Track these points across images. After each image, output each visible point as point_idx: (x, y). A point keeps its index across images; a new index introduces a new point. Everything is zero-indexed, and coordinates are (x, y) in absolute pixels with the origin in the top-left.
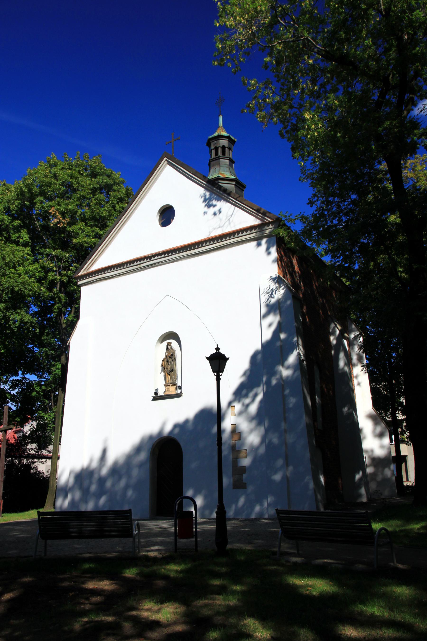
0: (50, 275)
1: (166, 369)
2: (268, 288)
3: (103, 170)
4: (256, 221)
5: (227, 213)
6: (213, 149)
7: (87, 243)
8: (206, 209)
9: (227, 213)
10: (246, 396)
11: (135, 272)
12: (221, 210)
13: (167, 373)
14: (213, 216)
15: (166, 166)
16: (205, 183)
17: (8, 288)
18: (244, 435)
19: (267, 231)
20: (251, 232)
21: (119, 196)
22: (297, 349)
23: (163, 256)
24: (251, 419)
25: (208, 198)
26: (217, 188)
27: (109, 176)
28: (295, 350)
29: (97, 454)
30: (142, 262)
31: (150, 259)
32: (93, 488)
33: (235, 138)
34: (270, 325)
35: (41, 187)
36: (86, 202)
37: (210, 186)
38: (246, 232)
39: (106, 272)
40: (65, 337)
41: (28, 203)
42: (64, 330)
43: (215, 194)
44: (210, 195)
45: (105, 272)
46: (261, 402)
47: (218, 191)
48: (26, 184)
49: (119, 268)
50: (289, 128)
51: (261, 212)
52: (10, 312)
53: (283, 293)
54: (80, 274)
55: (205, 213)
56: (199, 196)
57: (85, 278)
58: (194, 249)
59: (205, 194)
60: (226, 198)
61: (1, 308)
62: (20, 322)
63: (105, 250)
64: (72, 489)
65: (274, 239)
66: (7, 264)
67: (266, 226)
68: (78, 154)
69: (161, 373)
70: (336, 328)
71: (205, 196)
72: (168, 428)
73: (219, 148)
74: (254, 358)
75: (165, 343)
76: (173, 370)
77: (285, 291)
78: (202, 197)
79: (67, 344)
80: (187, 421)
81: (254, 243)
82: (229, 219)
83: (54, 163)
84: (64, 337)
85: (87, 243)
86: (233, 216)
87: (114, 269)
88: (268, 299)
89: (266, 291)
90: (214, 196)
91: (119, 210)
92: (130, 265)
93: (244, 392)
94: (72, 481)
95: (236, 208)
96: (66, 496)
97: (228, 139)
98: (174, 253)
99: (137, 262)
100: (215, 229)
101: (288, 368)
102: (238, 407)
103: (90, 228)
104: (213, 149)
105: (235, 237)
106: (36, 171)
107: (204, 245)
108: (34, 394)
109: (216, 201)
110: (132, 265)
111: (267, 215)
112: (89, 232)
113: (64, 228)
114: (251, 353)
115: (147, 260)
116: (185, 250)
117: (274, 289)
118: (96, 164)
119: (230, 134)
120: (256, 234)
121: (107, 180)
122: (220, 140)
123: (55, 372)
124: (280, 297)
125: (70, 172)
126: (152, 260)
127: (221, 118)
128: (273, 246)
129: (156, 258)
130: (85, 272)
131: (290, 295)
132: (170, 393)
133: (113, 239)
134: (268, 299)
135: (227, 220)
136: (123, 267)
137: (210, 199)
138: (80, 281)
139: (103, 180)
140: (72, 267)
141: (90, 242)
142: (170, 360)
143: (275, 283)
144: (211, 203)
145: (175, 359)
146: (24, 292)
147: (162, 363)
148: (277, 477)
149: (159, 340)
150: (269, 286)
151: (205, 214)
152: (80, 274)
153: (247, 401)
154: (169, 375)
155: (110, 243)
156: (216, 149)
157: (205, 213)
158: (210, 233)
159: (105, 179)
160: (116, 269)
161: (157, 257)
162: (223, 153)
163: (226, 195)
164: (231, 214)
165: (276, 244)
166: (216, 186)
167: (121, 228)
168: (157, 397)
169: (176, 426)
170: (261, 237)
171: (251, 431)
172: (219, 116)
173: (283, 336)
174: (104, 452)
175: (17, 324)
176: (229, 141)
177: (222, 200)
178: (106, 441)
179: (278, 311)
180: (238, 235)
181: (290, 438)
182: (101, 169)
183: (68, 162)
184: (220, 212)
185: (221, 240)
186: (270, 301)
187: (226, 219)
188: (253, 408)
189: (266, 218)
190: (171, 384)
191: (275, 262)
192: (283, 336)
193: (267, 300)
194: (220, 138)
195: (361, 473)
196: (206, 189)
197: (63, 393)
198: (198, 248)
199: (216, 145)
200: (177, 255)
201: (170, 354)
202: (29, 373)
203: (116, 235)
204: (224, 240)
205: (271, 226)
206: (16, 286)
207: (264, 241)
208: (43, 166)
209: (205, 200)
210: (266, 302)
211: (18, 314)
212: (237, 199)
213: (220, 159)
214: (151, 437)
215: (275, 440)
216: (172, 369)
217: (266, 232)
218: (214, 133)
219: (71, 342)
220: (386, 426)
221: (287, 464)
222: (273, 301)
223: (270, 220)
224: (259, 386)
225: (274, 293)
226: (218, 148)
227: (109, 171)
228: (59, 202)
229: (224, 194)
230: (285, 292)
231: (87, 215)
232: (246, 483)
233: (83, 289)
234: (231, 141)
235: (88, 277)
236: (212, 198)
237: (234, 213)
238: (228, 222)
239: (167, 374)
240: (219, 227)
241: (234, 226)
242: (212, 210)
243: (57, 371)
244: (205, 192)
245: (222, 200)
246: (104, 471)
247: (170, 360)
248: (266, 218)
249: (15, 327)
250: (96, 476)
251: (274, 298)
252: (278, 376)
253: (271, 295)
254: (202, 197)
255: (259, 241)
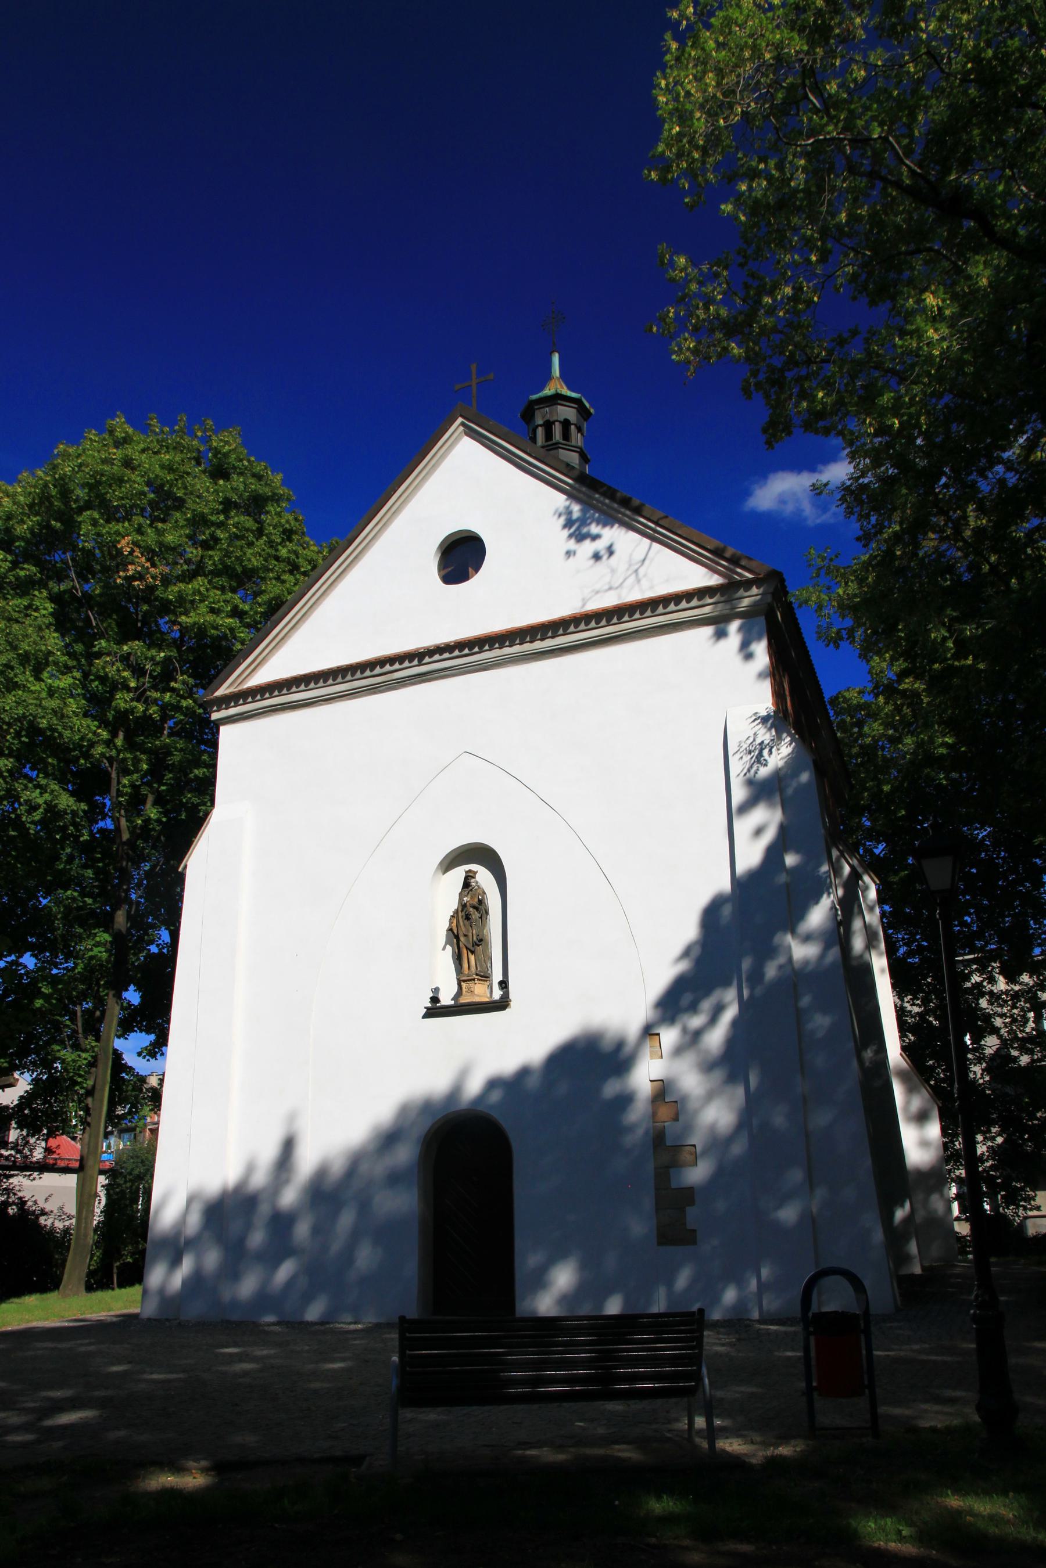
0: (120, 699)
1: (462, 939)
2: (751, 739)
3: (246, 463)
4: (711, 577)
5: (631, 555)
6: (541, 426)
7: (216, 628)
8: (572, 544)
9: (631, 555)
10: (693, 1008)
11: (375, 693)
12: (615, 548)
13: (467, 948)
14: (592, 561)
15: (461, 439)
16: (570, 481)
17: (19, 719)
18: (692, 1105)
19: (746, 602)
20: (700, 603)
21: (287, 526)
22: (829, 894)
23: (456, 653)
24: (708, 1067)
25: (577, 520)
26: (604, 495)
27: (259, 477)
28: (825, 896)
29: (268, 1152)
30: (397, 666)
31: (420, 661)
32: (257, 1238)
33: (591, 405)
34: (758, 832)
35: (91, 487)
36: (207, 532)
37: (584, 489)
38: (688, 602)
39: (294, 689)
40: (127, 865)
41: (59, 525)
42: (125, 847)
43: (596, 509)
44: (583, 511)
45: (292, 691)
46: (735, 1023)
47: (607, 501)
48: (57, 476)
49: (330, 682)
50: (762, 377)
51: (728, 555)
52: (22, 783)
53: (789, 755)
54: (218, 693)
55: (569, 554)
56: (552, 512)
57: (232, 704)
58: (542, 640)
59: (568, 508)
60: (627, 519)
61: (4, 769)
62: (45, 809)
63: (290, 637)
64: (191, 1243)
65: (761, 621)
66: (24, 659)
67: (742, 590)
68: (181, 419)
69: (444, 949)
70: (843, 861)
71: (569, 512)
72: (474, 1087)
73: (557, 424)
74: (711, 915)
75: (458, 874)
76: (481, 940)
77: (794, 749)
78: (560, 515)
79: (180, 870)
80: (524, 1072)
81: (708, 631)
82: (636, 571)
83: (123, 435)
84: (124, 864)
85: (216, 628)
86: (647, 562)
87: (316, 683)
88: (751, 767)
89: (744, 748)
90: (594, 514)
91: (289, 558)
92: (362, 673)
93: (686, 999)
94: (194, 1220)
95: (656, 546)
96: (176, 1262)
97: (576, 406)
98: (487, 647)
99: (381, 667)
100: (597, 592)
101: (807, 938)
102: (669, 1036)
103: (219, 593)
104: (541, 426)
105: (657, 612)
106: (80, 451)
107: (572, 629)
108: (39, 1003)
109: (600, 527)
110: (368, 673)
111: (743, 563)
112: (219, 602)
113: (152, 589)
114: (704, 899)
115: (410, 662)
116: (539, 637)
117: (766, 742)
118: (230, 446)
119: (583, 395)
120: (714, 608)
121: (254, 486)
122: (559, 407)
123: (90, 953)
124: (781, 764)
125: (168, 457)
126: (424, 662)
127: (556, 359)
128: (759, 639)
129: (437, 657)
130: (231, 690)
131: (808, 759)
132: (477, 999)
133: (311, 610)
134: (751, 767)
135: (630, 572)
136: (343, 678)
137: (583, 521)
138: (218, 711)
139: (245, 484)
140: (176, 682)
141: (221, 625)
142: (475, 915)
143: (770, 729)
144: (585, 530)
145: (487, 913)
146: (61, 735)
147: (451, 922)
148: (788, 1214)
149: (441, 863)
150: (755, 734)
151: (569, 557)
152: (220, 692)
153: (696, 1021)
154: (473, 952)
155: (304, 618)
156: (548, 426)
157: (569, 554)
158: (584, 603)
159: (251, 483)
160: (321, 684)
161: (440, 655)
162: (566, 436)
163: (628, 513)
164: (642, 557)
165: (766, 634)
166: (601, 490)
167: (336, 583)
168: (435, 1010)
169: (493, 1084)
170: (727, 615)
171: (710, 1096)
172: (553, 352)
173: (790, 860)
174: (288, 1146)
175: (37, 816)
176: (578, 411)
177: (617, 525)
178: (292, 1118)
179: (778, 799)
180: (665, 607)
181: (821, 1119)
182: (241, 460)
183: (160, 437)
184: (610, 551)
185: (619, 619)
186: (756, 773)
187: (628, 569)
188: (716, 1038)
189: (739, 570)
190: (477, 975)
191: (766, 677)
192: (790, 860)
193: (749, 770)
194: (559, 402)
195: (907, 1205)
196: (570, 495)
197: (117, 1003)
198: (553, 637)
199: (548, 417)
200: (496, 653)
201: (476, 900)
202: (15, 953)
203: (322, 599)
204: (626, 618)
205: (754, 590)
206: (43, 717)
207: (734, 626)
208: (95, 441)
209: (568, 524)
210: (745, 774)
211: (38, 791)
212: (661, 522)
213: (560, 450)
214: (427, 1106)
215: (779, 1120)
216: (480, 937)
217: (740, 603)
218: (542, 388)
219: (189, 864)
220: (932, 1097)
221: (811, 1182)
222: (764, 772)
223: (751, 576)
224: (726, 983)
225: (766, 752)
226: (554, 423)
227: (260, 467)
228: (140, 526)
229: (623, 510)
230: (792, 752)
231: (210, 562)
232: (694, 1231)
233: (224, 730)
234: (583, 412)
235: (241, 702)
236: (589, 518)
237: (651, 555)
238: (633, 578)
239: (465, 951)
240: (610, 589)
241: (652, 588)
242: (588, 547)
243: (96, 950)
244: (568, 503)
245: (617, 525)
246: (289, 1197)
247: (475, 915)
248: (739, 570)
249: (33, 822)
250: (264, 1209)
251: (766, 765)
252: (781, 960)
253: (757, 757)
254: (560, 515)
255: (722, 626)
